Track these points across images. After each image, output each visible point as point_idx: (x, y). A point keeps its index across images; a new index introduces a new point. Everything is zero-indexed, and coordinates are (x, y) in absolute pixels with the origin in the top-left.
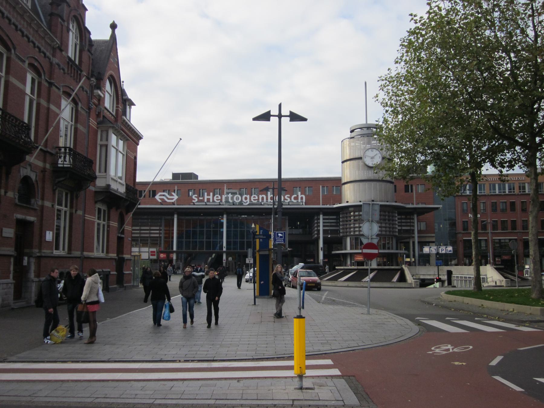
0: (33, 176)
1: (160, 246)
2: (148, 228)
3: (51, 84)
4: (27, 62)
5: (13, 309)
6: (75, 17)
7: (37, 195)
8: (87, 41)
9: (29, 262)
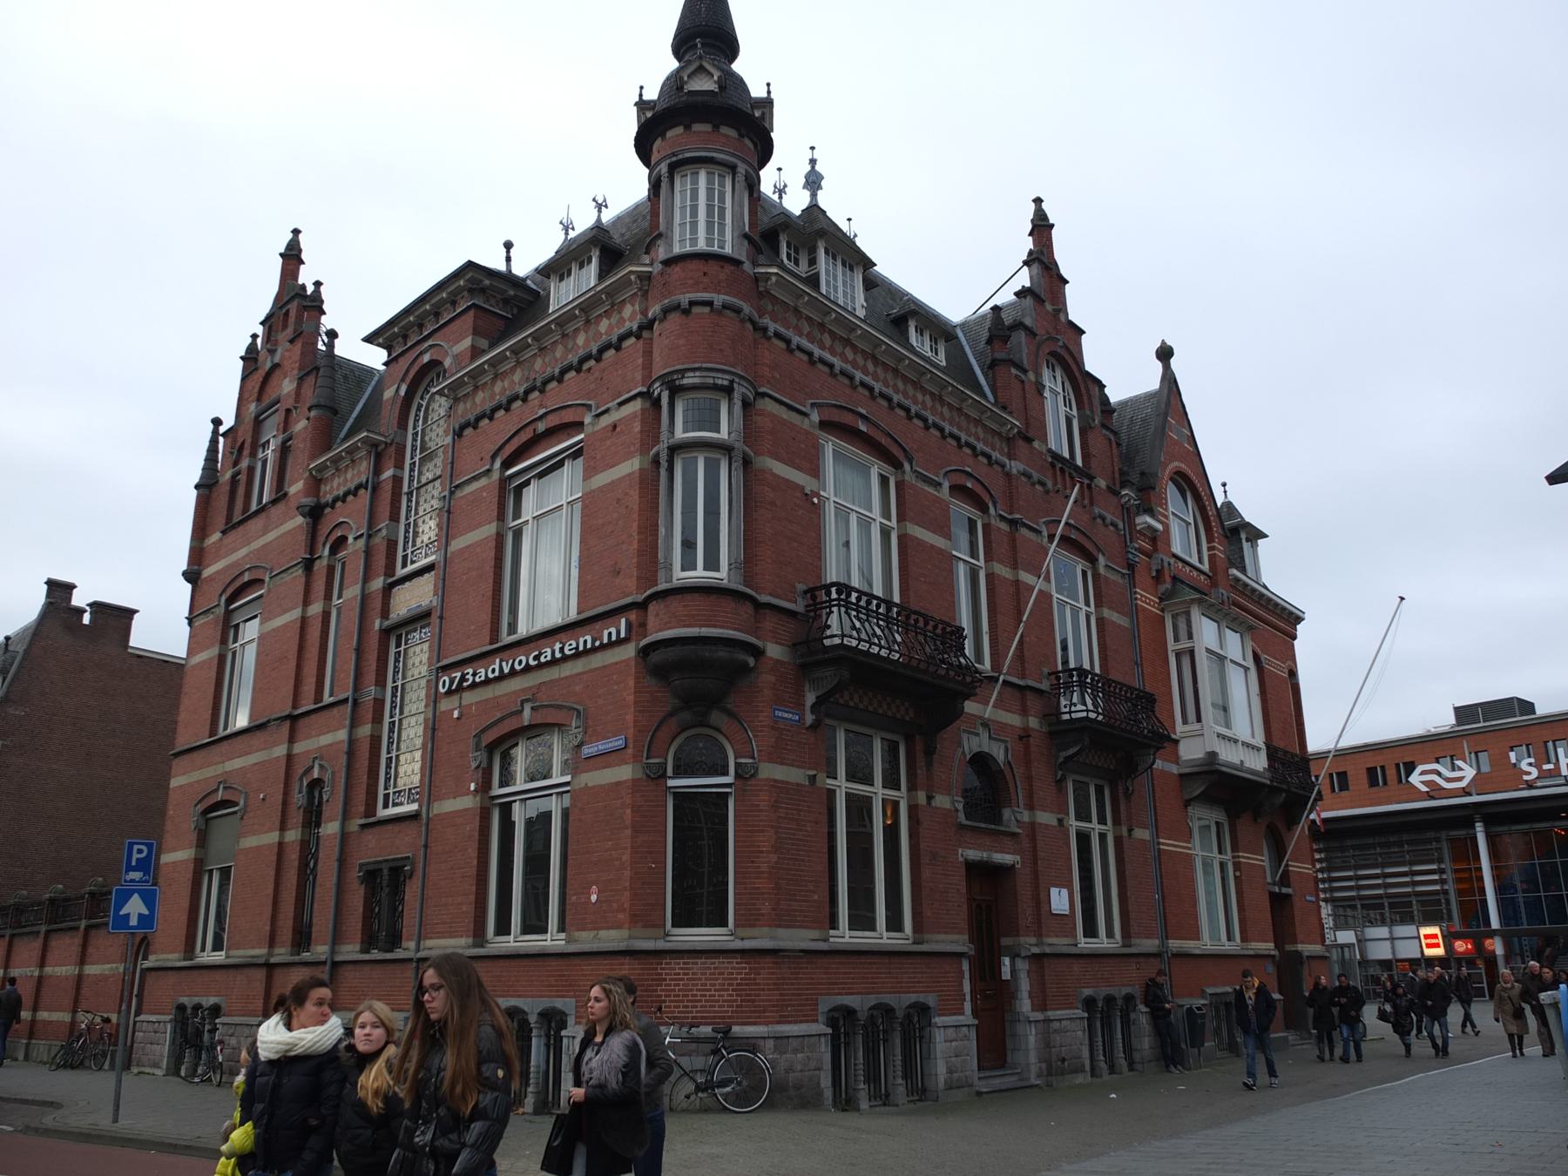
0: (998, 751)
1: (1450, 918)
2: (1405, 869)
3: (1013, 523)
4: (946, 485)
5: (979, 1094)
6: (1053, 354)
7: (1013, 797)
8: (1096, 402)
9: (1013, 971)
